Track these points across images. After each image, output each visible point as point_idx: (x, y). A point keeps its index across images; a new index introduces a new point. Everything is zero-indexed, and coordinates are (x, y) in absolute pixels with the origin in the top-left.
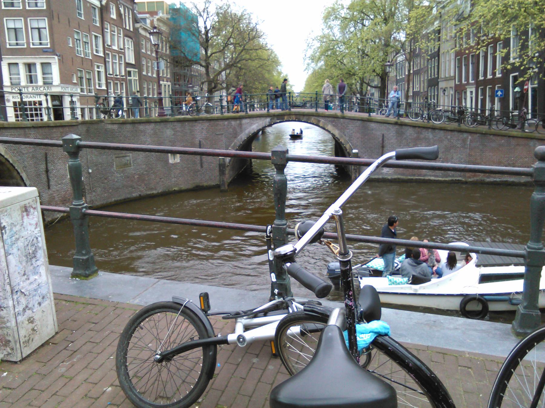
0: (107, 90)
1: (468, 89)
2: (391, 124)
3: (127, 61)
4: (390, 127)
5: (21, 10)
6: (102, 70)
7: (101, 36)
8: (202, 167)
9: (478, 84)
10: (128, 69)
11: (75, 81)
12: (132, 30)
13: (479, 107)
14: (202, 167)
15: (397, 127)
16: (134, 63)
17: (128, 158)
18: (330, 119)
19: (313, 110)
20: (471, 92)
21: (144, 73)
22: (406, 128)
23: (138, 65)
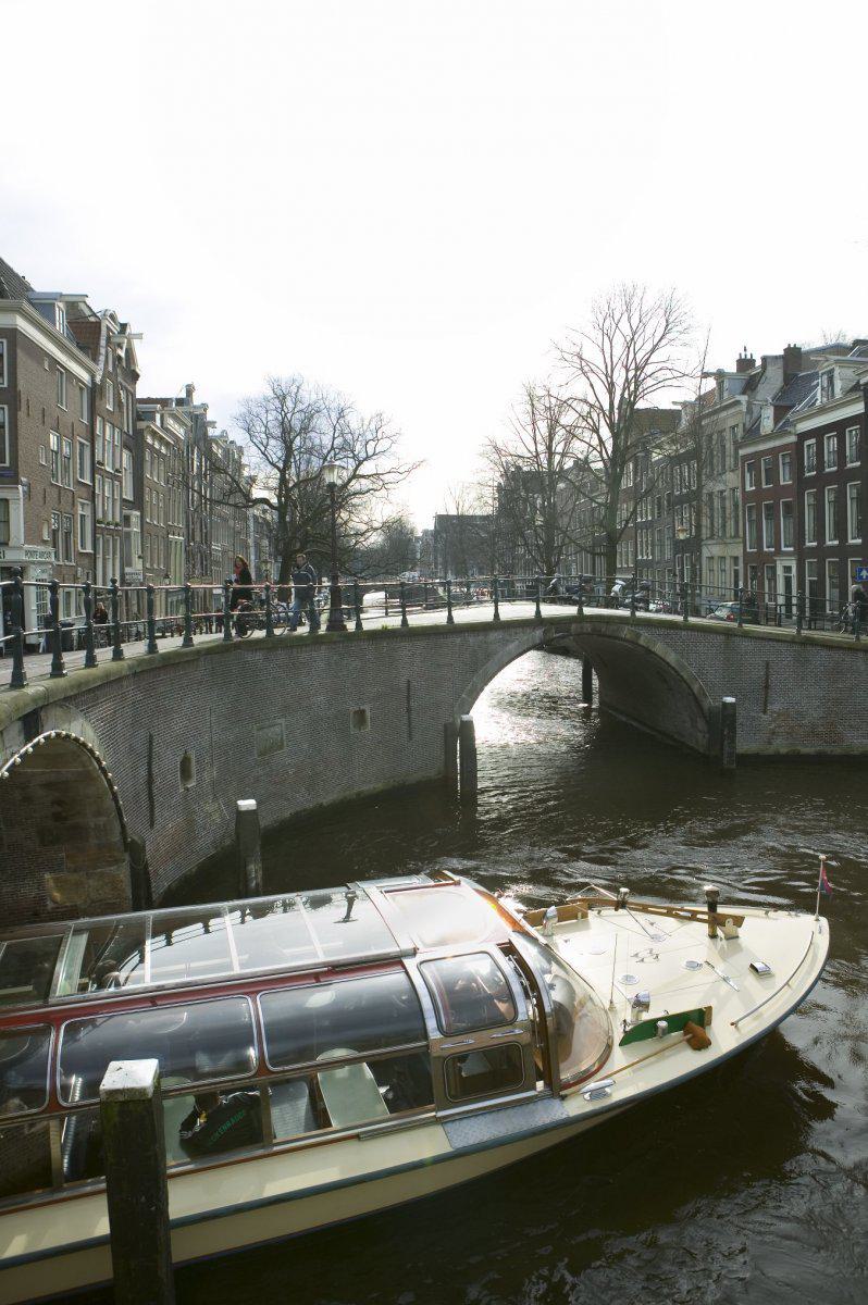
0: (95, 554)
1: (778, 562)
2: (785, 641)
3: (124, 497)
4: (783, 647)
5: (8, 342)
6: (88, 512)
7: (88, 444)
8: (410, 736)
9: (801, 554)
10: (126, 512)
11: (46, 538)
12: (131, 433)
13: (794, 592)
14: (410, 736)
15: (796, 647)
16: (131, 499)
17: (277, 729)
18: (662, 631)
19: (680, 618)
20: (787, 569)
21: (640, 557)
22: (814, 650)
23: (138, 502)
